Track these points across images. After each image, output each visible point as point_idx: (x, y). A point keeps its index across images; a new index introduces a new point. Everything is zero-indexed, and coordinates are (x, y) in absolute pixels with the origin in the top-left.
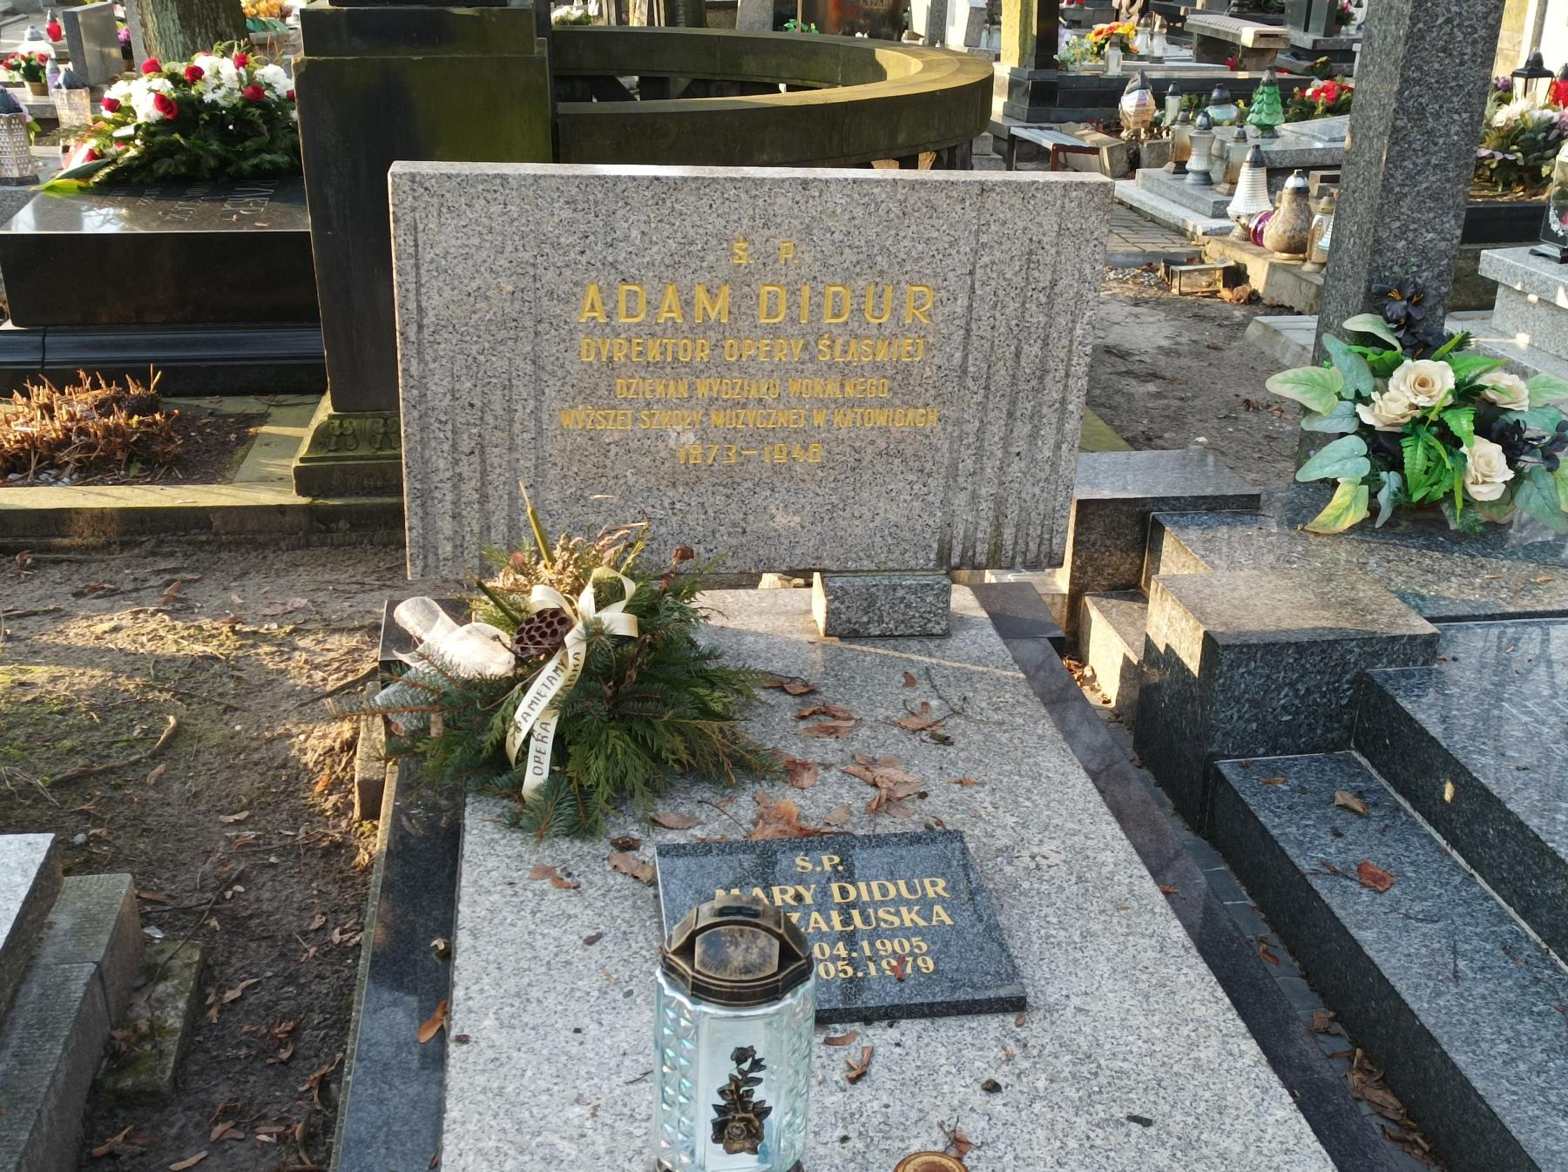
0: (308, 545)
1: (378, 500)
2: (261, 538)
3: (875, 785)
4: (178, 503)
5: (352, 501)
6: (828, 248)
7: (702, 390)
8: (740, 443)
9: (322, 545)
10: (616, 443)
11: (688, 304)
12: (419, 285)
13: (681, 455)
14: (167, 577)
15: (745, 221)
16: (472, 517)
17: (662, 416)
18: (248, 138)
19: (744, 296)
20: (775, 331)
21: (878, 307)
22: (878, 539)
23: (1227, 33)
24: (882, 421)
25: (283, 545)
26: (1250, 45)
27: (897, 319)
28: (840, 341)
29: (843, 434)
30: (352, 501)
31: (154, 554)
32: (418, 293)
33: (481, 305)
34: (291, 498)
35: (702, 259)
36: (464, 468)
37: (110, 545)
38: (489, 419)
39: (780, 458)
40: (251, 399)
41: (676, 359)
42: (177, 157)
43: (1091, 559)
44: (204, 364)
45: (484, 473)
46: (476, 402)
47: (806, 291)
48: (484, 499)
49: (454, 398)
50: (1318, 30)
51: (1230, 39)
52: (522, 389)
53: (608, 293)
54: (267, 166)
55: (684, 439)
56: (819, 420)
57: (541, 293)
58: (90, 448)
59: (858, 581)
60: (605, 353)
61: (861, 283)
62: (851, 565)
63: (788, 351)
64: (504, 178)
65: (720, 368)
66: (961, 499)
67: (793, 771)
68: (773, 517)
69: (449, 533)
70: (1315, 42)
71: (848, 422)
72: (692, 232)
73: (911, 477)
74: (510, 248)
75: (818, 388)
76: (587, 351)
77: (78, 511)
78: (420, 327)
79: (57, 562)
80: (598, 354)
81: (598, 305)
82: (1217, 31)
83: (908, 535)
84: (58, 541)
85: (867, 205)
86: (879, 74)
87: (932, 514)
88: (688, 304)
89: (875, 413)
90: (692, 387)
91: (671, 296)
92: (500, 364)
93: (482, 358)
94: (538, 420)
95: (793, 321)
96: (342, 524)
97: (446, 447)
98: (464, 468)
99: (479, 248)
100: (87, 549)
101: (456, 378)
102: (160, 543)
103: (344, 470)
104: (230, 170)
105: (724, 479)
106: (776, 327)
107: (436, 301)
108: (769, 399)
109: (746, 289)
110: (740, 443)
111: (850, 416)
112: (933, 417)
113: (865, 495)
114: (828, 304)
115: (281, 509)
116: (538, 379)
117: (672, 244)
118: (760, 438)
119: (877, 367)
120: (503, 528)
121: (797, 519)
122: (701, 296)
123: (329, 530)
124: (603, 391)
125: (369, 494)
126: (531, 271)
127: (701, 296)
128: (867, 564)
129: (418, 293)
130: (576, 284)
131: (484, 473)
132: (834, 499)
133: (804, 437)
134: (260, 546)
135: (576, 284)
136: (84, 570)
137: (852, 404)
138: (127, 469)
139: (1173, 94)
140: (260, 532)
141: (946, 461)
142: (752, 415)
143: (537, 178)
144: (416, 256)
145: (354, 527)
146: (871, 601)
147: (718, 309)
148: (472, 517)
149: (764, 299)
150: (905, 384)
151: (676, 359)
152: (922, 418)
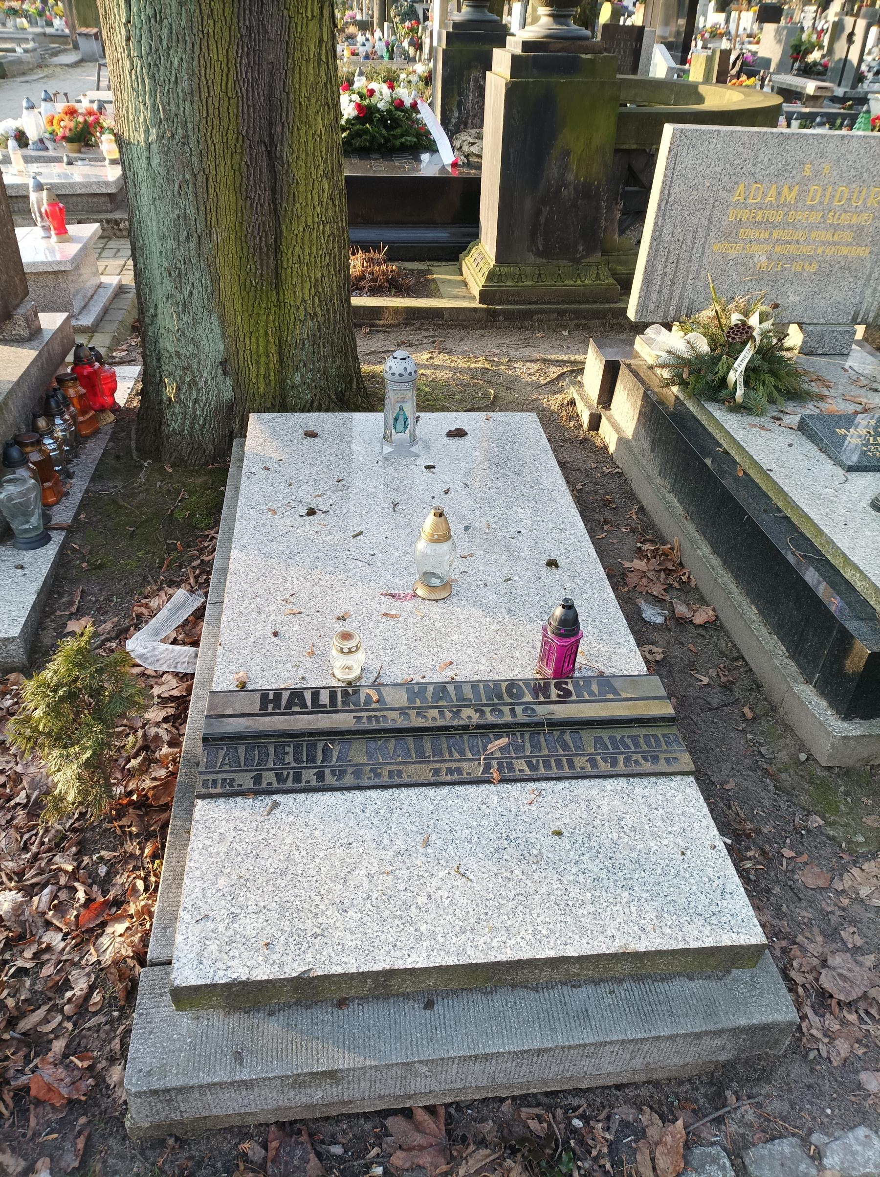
0: (486, 327)
1: (517, 307)
2: (465, 323)
3: (860, 404)
4: (428, 306)
5: (505, 307)
6: (845, 169)
7: (775, 235)
8: (784, 261)
9: (492, 327)
10: (732, 259)
11: (779, 194)
12: (672, 182)
13: (758, 266)
14: (431, 339)
15: (813, 155)
16: (666, 292)
17: (755, 247)
18: (396, 128)
19: (804, 191)
20: (812, 208)
21: (858, 198)
22: (829, 309)
23: (797, 87)
24: (845, 253)
25: (475, 327)
26: (812, 93)
27: (864, 203)
28: (838, 214)
29: (828, 258)
30: (505, 307)
31: (420, 329)
32: (670, 186)
33: (695, 192)
34: (476, 304)
35: (791, 173)
36: (668, 270)
37: (400, 324)
38: (684, 246)
39: (799, 269)
40: (416, 263)
41: (767, 220)
42: (364, 137)
43: (872, 334)
44: (396, 245)
45: (676, 272)
46: (681, 239)
47: (830, 189)
48: (673, 284)
49: (673, 237)
50: (846, 86)
51: (799, 90)
52: (701, 233)
53: (747, 188)
54: (408, 143)
55: (761, 259)
56: (820, 251)
57: (720, 187)
58: (374, 280)
59: (819, 328)
60: (739, 217)
61: (854, 186)
62: (815, 321)
63: (816, 217)
64: (719, 132)
65: (784, 225)
66: (869, 291)
67: (822, 398)
68: (789, 297)
69: (654, 300)
70: (845, 92)
71: (831, 253)
72: (789, 159)
73: (851, 280)
74: (713, 165)
75: (823, 236)
76: (732, 215)
77: (387, 308)
78: (667, 202)
79: (379, 332)
80: (736, 217)
81: (742, 193)
82: (791, 85)
83: (842, 307)
84: (377, 322)
85: (866, 148)
86: (701, 99)
87: (855, 298)
88: (779, 194)
89: (844, 248)
90: (771, 234)
91: (773, 191)
92: (695, 220)
93: (688, 218)
94: (704, 248)
95: (821, 203)
96: (501, 318)
97: (663, 260)
98: (668, 270)
99: (700, 165)
100: (390, 326)
101: (675, 227)
102: (422, 324)
103: (502, 292)
104: (389, 144)
105: (773, 278)
106: (813, 206)
107: (677, 190)
108: (801, 240)
109: (805, 188)
110: (784, 261)
111: (833, 249)
112: (867, 251)
113: (829, 288)
114: (838, 195)
115: (475, 310)
116: (709, 228)
117: (780, 165)
118: (792, 259)
119: (850, 227)
120: (677, 299)
121: (798, 298)
122: (786, 190)
123: (495, 321)
124: (733, 235)
125: (511, 304)
126: (719, 176)
127: (786, 190)
128: (822, 321)
129: (670, 186)
130: (736, 183)
131: (676, 272)
132: (816, 289)
133: (810, 259)
134: (465, 327)
135: (736, 183)
136: (391, 335)
137: (835, 244)
138: (390, 291)
139: (796, 119)
140: (465, 320)
141: (867, 272)
142: (792, 248)
143: (732, 132)
144: (674, 169)
145: (506, 320)
146: (822, 337)
147: (790, 196)
148: (666, 292)
149: (811, 192)
150: (860, 235)
151: (767, 220)
152: (863, 252)
